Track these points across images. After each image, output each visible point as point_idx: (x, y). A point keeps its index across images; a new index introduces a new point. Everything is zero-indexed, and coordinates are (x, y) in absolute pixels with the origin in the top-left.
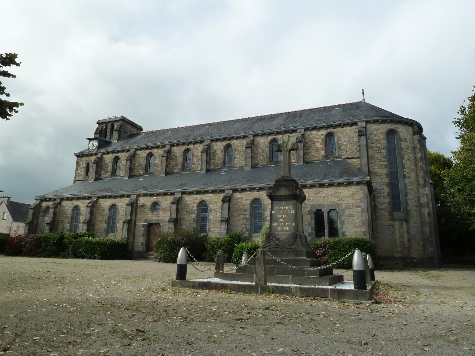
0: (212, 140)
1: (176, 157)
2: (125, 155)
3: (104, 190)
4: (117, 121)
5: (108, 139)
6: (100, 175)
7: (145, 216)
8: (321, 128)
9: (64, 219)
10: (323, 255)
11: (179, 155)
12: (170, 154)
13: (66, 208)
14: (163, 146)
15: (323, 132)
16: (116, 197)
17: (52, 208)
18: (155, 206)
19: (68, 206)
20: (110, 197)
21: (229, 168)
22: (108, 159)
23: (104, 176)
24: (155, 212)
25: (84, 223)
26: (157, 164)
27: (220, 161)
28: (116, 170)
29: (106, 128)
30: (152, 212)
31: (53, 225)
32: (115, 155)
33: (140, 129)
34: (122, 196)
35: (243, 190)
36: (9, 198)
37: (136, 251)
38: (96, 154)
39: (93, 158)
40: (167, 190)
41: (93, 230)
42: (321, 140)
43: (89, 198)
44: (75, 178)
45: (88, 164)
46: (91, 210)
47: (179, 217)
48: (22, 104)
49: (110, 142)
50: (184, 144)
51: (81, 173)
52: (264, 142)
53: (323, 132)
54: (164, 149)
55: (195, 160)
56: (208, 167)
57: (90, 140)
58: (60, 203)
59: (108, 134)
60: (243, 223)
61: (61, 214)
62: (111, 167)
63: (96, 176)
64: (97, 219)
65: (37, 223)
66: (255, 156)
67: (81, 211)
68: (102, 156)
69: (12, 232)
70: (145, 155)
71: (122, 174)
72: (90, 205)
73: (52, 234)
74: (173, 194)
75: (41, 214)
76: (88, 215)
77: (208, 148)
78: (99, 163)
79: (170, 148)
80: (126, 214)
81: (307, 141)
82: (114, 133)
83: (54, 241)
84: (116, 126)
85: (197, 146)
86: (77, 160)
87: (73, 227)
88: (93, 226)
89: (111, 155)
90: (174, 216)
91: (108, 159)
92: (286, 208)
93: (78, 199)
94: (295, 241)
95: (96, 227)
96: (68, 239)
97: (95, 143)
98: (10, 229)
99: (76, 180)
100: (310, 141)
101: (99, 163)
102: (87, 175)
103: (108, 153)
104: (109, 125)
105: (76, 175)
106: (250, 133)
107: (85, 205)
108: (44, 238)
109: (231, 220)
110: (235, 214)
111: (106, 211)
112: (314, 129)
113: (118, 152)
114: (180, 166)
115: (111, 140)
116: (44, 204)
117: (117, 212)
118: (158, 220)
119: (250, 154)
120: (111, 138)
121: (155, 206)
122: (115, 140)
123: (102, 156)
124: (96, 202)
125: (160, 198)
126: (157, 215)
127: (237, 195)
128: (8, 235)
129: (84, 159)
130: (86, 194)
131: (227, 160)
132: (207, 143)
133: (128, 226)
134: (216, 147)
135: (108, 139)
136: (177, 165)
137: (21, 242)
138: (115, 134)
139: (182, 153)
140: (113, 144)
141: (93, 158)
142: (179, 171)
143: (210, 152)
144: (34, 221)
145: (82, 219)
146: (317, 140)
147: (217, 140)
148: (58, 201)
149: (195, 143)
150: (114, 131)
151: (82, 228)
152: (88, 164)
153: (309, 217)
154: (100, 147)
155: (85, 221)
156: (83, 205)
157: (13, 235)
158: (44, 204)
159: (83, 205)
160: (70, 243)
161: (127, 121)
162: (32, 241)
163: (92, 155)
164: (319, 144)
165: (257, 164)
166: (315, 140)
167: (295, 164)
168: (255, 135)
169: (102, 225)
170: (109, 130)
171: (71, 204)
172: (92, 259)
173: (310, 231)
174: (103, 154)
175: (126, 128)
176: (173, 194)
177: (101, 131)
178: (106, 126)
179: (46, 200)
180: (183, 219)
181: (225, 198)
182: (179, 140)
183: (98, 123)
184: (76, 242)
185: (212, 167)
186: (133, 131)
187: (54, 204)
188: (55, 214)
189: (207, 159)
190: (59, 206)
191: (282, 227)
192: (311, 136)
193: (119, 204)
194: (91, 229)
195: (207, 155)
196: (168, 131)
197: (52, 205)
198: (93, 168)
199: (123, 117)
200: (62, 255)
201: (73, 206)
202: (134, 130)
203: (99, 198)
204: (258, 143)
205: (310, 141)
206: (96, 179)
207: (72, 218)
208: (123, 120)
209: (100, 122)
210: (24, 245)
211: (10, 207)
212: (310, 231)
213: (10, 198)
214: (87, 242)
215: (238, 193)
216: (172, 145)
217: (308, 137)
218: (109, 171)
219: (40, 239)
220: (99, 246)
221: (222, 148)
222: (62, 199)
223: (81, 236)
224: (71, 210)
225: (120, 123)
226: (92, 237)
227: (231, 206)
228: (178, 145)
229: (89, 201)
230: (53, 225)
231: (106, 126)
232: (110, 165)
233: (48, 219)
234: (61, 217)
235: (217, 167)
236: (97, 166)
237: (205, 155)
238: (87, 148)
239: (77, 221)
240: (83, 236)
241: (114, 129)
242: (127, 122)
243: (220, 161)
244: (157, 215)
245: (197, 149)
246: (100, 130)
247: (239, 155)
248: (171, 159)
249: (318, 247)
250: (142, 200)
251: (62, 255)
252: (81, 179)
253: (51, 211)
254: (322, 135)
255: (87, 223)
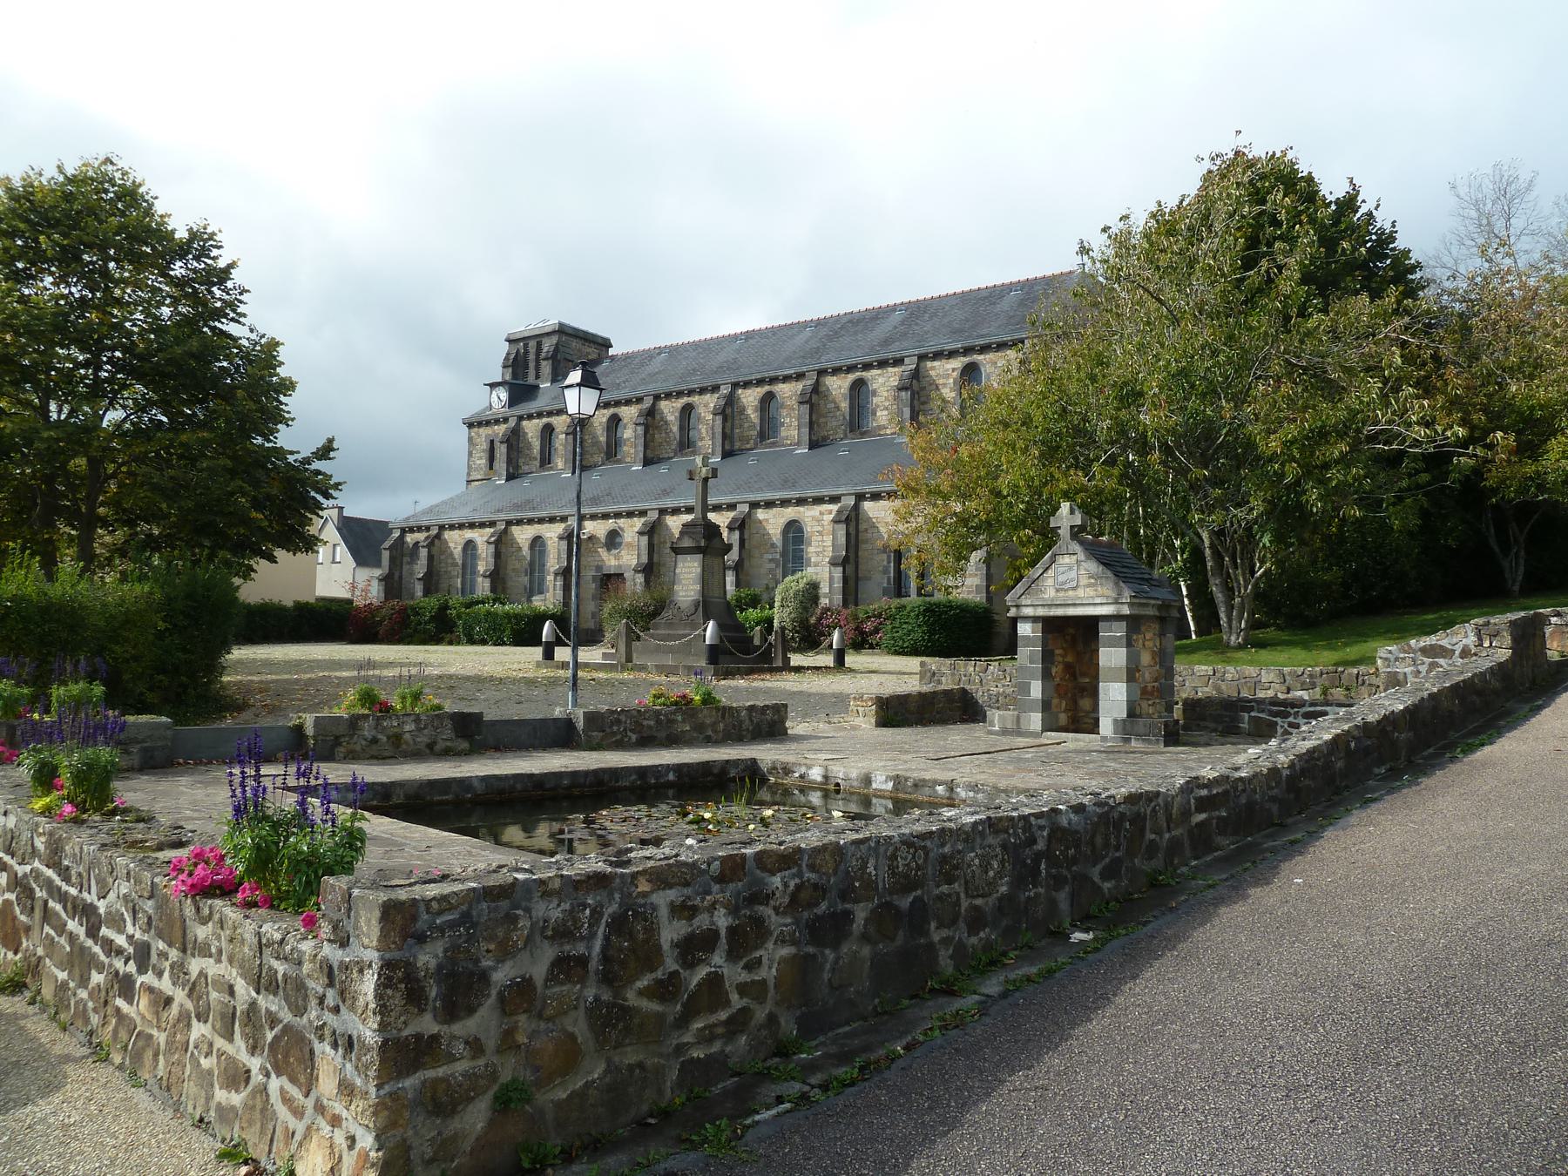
0: (735, 385)
1: (666, 422)
2: (565, 421)
3: (517, 507)
4: (548, 334)
5: (531, 380)
6: (517, 467)
7: (597, 558)
8: (952, 354)
9: (449, 569)
10: (877, 631)
11: (671, 418)
12: (654, 418)
13: (451, 545)
14: (639, 400)
15: (958, 363)
16: (541, 521)
17: (423, 547)
18: (613, 539)
19: (455, 540)
20: (530, 521)
21: (770, 447)
22: (532, 428)
23: (525, 468)
24: (614, 552)
25: (485, 576)
26: (628, 439)
27: (752, 433)
28: (549, 455)
29: (526, 352)
30: (609, 550)
31: (431, 581)
32: (545, 420)
33: (606, 344)
34: (552, 520)
35: (769, 504)
36: (341, 509)
37: (248, 607)
38: (506, 420)
39: (501, 429)
40: (631, 506)
41: (504, 590)
42: (951, 381)
43: (492, 524)
44: (469, 474)
45: (492, 442)
46: (496, 548)
47: (656, 559)
48: (345, 482)
49: (537, 387)
50: (680, 394)
51: (478, 462)
52: (840, 388)
53: (958, 363)
54: (639, 406)
55: (703, 431)
56: (727, 447)
57: (493, 386)
58: (438, 536)
59: (532, 365)
60: (771, 570)
61: (442, 557)
62: (538, 448)
63: (508, 470)
64: (510, 567)
65: (401, 577)
66: (822, 420)
67: (480, 551)
68: (518, 424)
69: (358, 593)
70: (605, 420)
71: (560, 465)
72: (493, 539)
73: (427, 599)
74: (643, 513)
75: (406, 559)
76: (491, 561)
77: (726, 404)
78: (514, 440)
79: (654, 405)
80: (559, 558)
81: (924, 383)
82: (544, 363)
83: (430, 612)
84: (548, 345)
85: (707, 397)
86: (470, 433)
87: (469, 586)
88: (504, 581)
89: (536, 421)
90: (645, 559)
91: (532, 428)
92: (691, 565)
93: (472, 526)
94: (696, 610)
95: (510, 584)
96: (455, 608)
97: (503, 395)
98: (353, 587)
99: (472, 478)
100: (931, 384)
101: (514, 440)
102: (491, 468)
103: (530, 417)
104: (532, 344)
105: (469, 467)
106: (811, 366)
107: (485, 538)
108: (413, 609)
109: (746, 564)
110: (756, 553)
111: (526, 551)
112: (938, 355)
113: (550, 414)
114: (674, 445)
115: (538, 382)
116: (410, 539)
117: (544, 551)
118: (620, 566)
119: (807, 416)
120: (537, 377)
121: (613, 539)
122: (546, 382)
123: (518, 424)
124: (505, 531)
125: (622, 522)
126: (617, 557)
127: (761, 514)
128: (350, 602)
129: (484, 431)
130: (486, 517)
131: (768, 428)
132: (725, 390)
133: (565, 580)
134: (744, 400)
135: (531, 380)
136: (668, 443)
137: (374, 617)
138: (546, 367)
139: (677, 414)
140: (541, 391)
141: (501, 429)
142: (672, 455)
143: (733, 412)
144: (393, 574)
145: (481, 568)
146: (945, 381)
147: (747, 385)
148: (434, 531)
149: (702, 391)
150: (543, 359)
151: (483, 587)
152: (492, 442)
153: (885, 556)
154: (513, 401)
155: (485, 571)
156: (481, 537)
157: (359, 602)
158: (410, 539)
159: (481, 537)
160: (459, 617)
161: (570, 332)
162: (392, 614)
163: (497, 422)
164: (948, 390)
165: (825, 439)
166: (941, 381)
167: (894, 438)
168: (822, 372)
169: (520, 579)
170: (532, 357)
171: (460, 536)
172: (499, 645)
173: (885, 585)
174: (521, 418)
175: (568, 350)
176: (643, 513)
177: (515, 359)
178: (526, 346)
179: (411, 530)
180: (664, 565)
181: (734, 520)
182: (671, 386)
183: (508, 340)
184: (468, 614)
185: (737, 445)
186: (588, 353)
187: (427, 538)
188: (430, 558)
189: (723, 428)
190: (436, 541)
191: (686, 591)
192: (932, 373)
193: (548, 535)
194: (500, 588)
195: (725, 420)
196: (659, 354)
197: (424, 541)
198: (501, 450)
199: (561, 324)
200: (447, 640)
201: (463, 542)
202: (590, 350)
203: (509, 523)
204: (828, 389)
205: (931, 384)
206: (510, 477)
207: (464, 565)
208: (563, 331)
209: (511, 338)
210: (380, 622)
211: (345, 531)
212: (885, 585)
213: (342, 508)
214: (489, 613)
215: (760, 510)
216: (657, 398)
217: (926, 374)
218: (535, 459)
219: (405, 609)
220: (510, 622)
221: (756, 403)
222: (442, 528)
223: (478, 603)
224: (460, 548)
225: (554, 339)
226: (501, 603)
227: (746, 537)
228: (668, 396)
229: (492, 530)
230: (431, 581)
231: (526, 346)
232: (536, 445)
233: (420, 568)
234: (443, 565)
235: (748, 446)
236: (510, 448)
237: (719, 419)
238: (488, 404)
239: (474, 572)
240: (483, 602)
241: (543, 355)
242: (570, 335)
243: (752, 433)
244: (617, 557)
245: (706, 406)
246: (512, 356)
247: (791, 418)
248: (657, 427)
249: (869, 617)
250: (590, 527)
251: (447, 640)
252: (480, 477)
253: (423, 552)
254: (954, 370)
255: (490, 576)
